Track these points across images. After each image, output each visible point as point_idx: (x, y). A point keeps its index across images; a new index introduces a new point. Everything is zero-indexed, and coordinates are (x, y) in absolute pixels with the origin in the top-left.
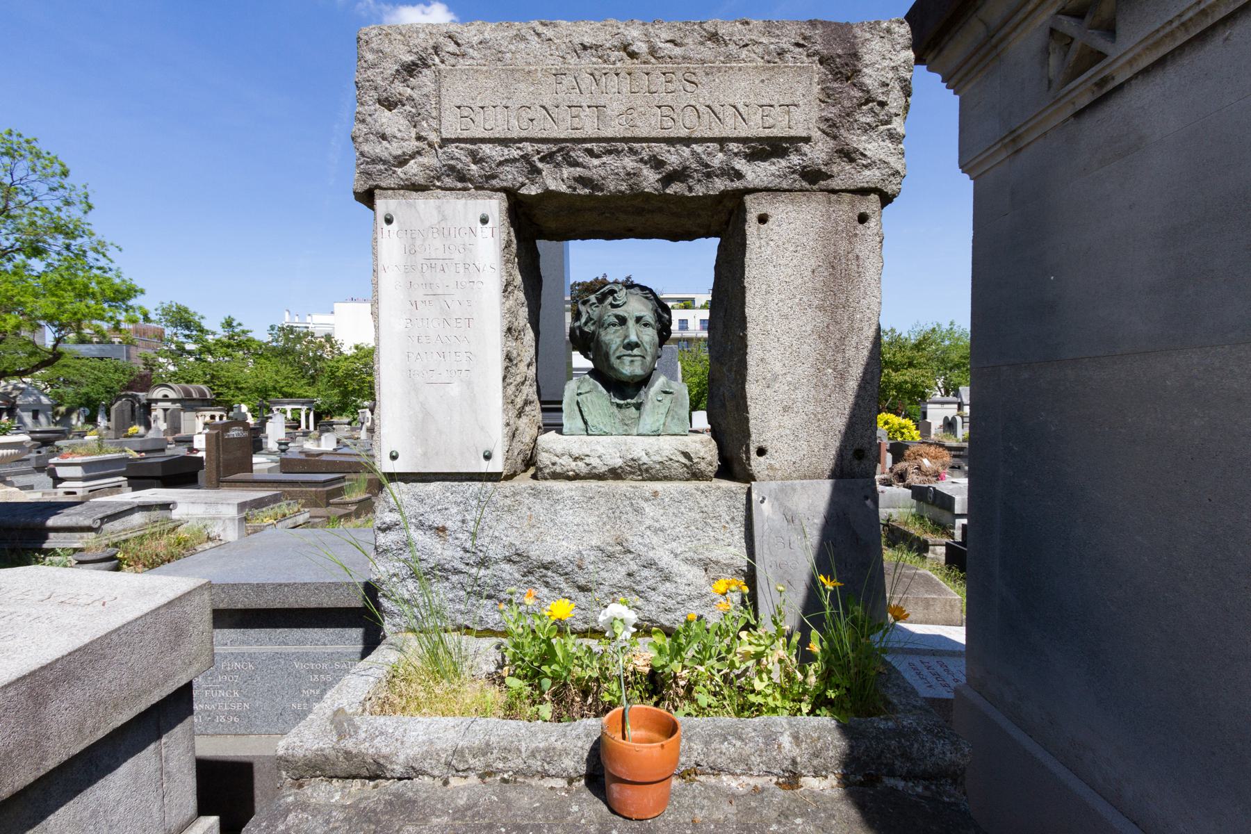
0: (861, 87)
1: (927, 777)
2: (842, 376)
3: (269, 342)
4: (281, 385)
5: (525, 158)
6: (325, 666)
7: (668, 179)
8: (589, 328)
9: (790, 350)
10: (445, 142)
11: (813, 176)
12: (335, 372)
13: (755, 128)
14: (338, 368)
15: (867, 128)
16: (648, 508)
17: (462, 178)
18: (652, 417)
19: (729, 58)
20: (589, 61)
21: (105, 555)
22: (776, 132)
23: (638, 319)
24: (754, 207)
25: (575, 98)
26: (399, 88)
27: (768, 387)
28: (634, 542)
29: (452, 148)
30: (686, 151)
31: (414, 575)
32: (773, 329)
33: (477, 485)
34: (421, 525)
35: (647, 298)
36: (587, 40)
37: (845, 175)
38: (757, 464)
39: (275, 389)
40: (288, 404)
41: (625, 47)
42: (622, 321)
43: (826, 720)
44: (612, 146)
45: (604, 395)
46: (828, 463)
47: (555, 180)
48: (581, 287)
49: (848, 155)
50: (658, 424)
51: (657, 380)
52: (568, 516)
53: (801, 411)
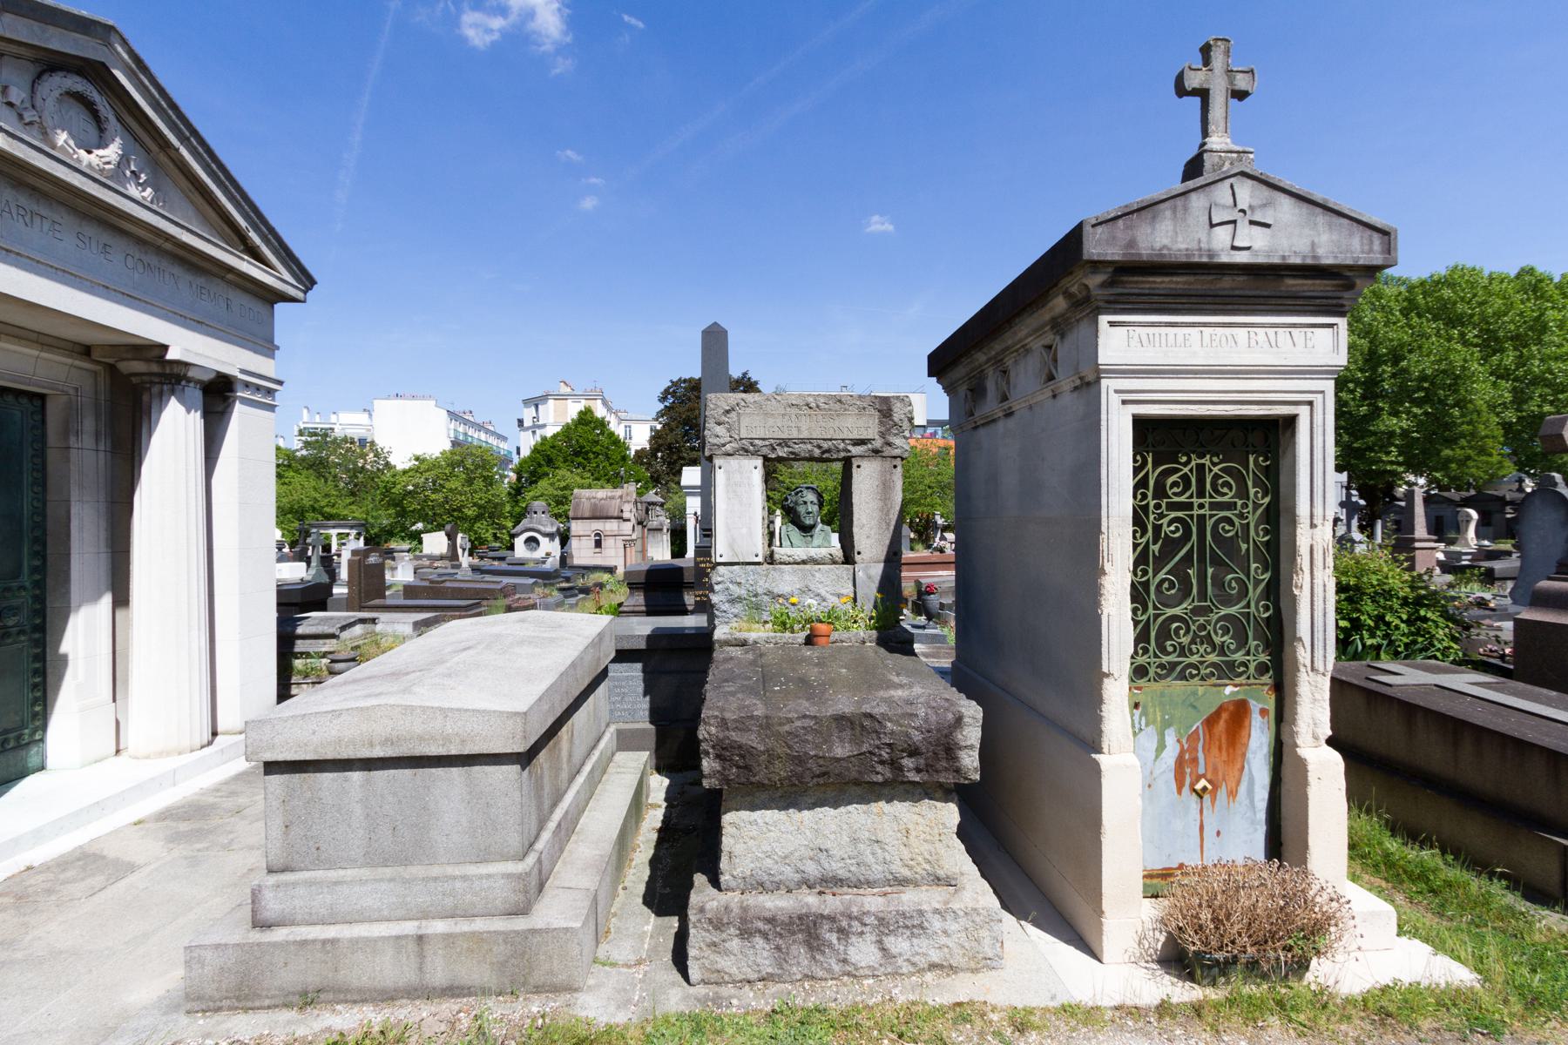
0: (893, 420)
1: (899, 643)
2: (888, 525)
3: (297, 450)
4: (323, 504)
5: (771, 445)
6: (624, 683)
7: (823, 453)
8: (791, 505)
10: (741, 439)
11: (876, 452)
12: (391, 488)
13: (855, 436)
15: (895, 435)
16: (817, 575)
17: (747, 451)
18: (817, 540)
19: (845, 410)
20: (794, 411)
21: (349, 657)
22: (862, 437)
24: (855, 462)
25: (790, 424)
26: (724, 418)
28: (812, 587)
29: (744, 441)
30: (830, 443)
31: (729, 601)
33: (752, 567)
34: (731, 582)
36: (794, 402)
37: (888, 451)
38: (857, 558)
39: (314, 509)
40: (334, 527)
41: (807, 405)
42: (805, 503)
43: (874, 632)
44: (803, 441)
46: (883, 558)
47: (782, 452)
48: (687, 384)
49: (889, 444)
52: (787, 577)
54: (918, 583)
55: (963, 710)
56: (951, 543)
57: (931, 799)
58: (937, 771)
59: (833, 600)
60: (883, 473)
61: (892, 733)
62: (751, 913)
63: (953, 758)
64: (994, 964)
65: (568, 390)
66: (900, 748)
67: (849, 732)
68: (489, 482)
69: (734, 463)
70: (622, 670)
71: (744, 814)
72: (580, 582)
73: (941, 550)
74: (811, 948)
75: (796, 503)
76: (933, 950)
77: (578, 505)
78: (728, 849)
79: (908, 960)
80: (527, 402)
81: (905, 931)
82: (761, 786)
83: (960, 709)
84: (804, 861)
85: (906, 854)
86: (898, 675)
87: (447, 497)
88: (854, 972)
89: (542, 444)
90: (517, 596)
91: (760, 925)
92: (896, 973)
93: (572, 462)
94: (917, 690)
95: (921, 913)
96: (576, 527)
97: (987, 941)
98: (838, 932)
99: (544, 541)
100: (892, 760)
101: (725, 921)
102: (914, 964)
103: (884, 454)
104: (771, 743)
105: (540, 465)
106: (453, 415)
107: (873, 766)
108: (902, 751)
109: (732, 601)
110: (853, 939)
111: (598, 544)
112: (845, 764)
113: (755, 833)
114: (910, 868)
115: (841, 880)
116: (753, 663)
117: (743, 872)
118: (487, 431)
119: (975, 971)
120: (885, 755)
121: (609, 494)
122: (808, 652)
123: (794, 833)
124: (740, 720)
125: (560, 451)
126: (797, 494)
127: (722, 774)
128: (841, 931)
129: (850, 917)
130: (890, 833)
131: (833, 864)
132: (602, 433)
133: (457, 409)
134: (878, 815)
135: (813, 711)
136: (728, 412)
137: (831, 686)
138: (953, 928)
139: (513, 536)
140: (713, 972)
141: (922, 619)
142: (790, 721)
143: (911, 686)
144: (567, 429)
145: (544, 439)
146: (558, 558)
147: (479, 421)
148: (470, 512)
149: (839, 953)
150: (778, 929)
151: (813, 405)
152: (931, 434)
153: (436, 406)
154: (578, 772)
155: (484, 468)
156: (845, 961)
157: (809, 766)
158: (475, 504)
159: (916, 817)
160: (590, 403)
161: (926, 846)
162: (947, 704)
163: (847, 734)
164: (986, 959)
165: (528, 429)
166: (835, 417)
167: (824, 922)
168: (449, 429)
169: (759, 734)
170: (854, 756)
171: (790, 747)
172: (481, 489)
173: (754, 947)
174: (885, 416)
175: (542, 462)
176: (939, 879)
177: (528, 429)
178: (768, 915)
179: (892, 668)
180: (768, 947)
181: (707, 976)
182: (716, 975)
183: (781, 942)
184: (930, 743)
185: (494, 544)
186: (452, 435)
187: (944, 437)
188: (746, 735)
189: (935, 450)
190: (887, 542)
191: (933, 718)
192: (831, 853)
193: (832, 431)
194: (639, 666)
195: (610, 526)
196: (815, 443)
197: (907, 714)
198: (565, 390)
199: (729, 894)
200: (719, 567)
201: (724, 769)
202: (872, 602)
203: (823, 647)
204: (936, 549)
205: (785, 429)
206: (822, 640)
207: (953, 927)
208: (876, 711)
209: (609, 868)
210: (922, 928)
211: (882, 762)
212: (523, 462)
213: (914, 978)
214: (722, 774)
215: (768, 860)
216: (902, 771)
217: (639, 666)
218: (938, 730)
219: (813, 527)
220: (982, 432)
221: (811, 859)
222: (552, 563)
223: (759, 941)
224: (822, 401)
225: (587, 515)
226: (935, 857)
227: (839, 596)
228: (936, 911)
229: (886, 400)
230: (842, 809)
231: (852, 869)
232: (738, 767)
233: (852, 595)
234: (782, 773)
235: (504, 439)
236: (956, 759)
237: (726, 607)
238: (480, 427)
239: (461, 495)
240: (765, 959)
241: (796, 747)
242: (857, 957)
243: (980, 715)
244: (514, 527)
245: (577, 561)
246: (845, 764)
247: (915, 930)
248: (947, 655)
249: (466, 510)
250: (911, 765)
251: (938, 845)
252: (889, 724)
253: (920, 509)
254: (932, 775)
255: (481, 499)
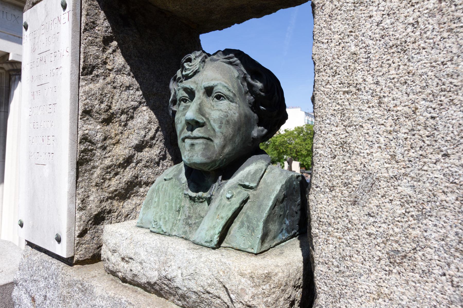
9: (409, 123)
14: (276, 141)
23: (209, 91)
27: (354, 203)
32: (370, 79)
35: (230, 63)
45: (181, 183)
50: (212, 232)
51: (248, 165)
53: (437, 271)
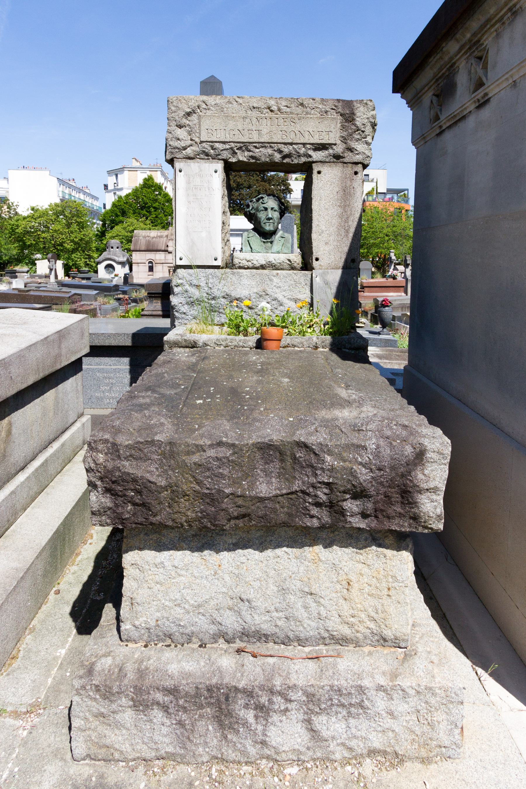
0: (355, 125)
2: (347, 231)
5: (232, 148)
6: (112, 375)
7: (284, 157)
10: (202, 142)
11: (337, 157)
12: (15, 229)
13: (316, 140)
15: (358, 140)
16: (275, 280)
17: (207, 155)
18: (276, 246)
19: (307, 113)
20: (255, 114)
26: (185, 121)
28: (269, 291)
29: (204, 144)
30: (291, 147)
31: (187, 303)
34: (191, 284)
37: (349, 157)
38: (315, 264)
41: (269, 108)
42: (266, 209)
44: (263, 145)
46: (341, 264)
47: (243, 156)
49: (351, 150)
54: (376, 300)
55: (426, 442)
56: (402, 273)
57: (380, 546)
58: (389, 517)
59: (290, 305)
60: (343, 179)
61: (332, 469)
62: (149, 681)
63: (410, 503)
64: (451, 753)
65: (137, 164)
66: (342, 489)
67: (277, 464)
68: (82, 226)
69: (194, 166)
70: (111, 363)
71: (149, 555)
72: (134, 295)
73: (394, 278)
74: (221, 725)
75: (257, 210)
76: (374, 733)
77: (137, 241)
78: (129, 594)
79: (343, 744)
80: (110, 173)
81: (340, 710)
82: (162, 526)
83: (422, 440)
84: (222, 611)
85: (346, 609)
86: (347, 387)
87: (52, 236)
88: (275, 756)
89: (118, 201)
90: (82, 303)
91: (159, 697)
92: (328, 759)
93: (139, 214)
94: (368, 410)
95: (361, 689)
96: (136, 257)
97: (443, 727)
98: (256, 709)
99: (118, 267)
100: (330, 502)
101: (115, 689)
102: (351, 749)
103: (345, 160)
104: (175, 476)
105: (117, 216)
106: (61, 182)
107: (306, 508)
108: (344, 492)
109: (191, 304)
110: (275, 718)
111: (151, 269)
112: (270, 505)
113: (161, 578)
114: (351, 626)
115: (266, 636)
116: (192, 367)
117: (146, 622)
118: (85, 193)
119: (425, 761)
120: (322, 495)
121: (159, 234)
122: (255, 357)
123: (210, 578)
124: (137, 447)
125: (130, 206)
126: (258, 200)
127: (114, 512)
128: (259, 707)
129: (272, 692)
130: (327, 585)
131: (256, 617)
132: (160, 194)
133: (64, 177)
134: (314, 561)
135: (231, 438)
136: (189, 114)
137: (264, 401)
138: (400, 709)
139: (99, 263)
140: (101, 747)
141: (378, 327)
142: (201, 449)
143: (360, 403)
144: (136, 191)
145: (120, 197)
146: (122, 278)
147: (79, 186)
148: (69, 246)
149: (256, 734)
150: (181, 702)
151: (274, 108)
152: (389, 198)
153: (50, 175)
154: (23, 469)
155: (78, 217)
156: (263, 743)
157: (224, 506)
158: (72, 241)
159: (361, 566)
160: (153, 174)
161: (372, 601)
162: (404, 433)
163: (275, 466)
164: (440, 747)
165: (111, 191)
166: (297, 121)
167: (240, 696)
168: (58, 191)
169: (161, 465)
170: (282, 495)
171: (199, 483)
172: (76, 231)
173: (151, 721)
174: (347, 121)
175: (119, 214)
176: (385, 640)
177: (111, 191)
178: (169, 683)
179: (342, 379)
180: (168, 722)
181: (94, 750)
182: (104, 750)
183: (184, 717)
184: (381, 483)
185: (84, 269)
186: (61, 195)
187: (398, 201)
188: (144, 465)
189: (392, 209)
190: (346, 249)
191: (386, 452)
192: (254, 604)
193: (292, 135)
194: (126, 360)
195: (159, 257)
196: (276, 147)
197: (353, 445)
198: (136, 164)
199: (130, 645)
200: (179, 271)
201: (117, 505)
202: (329, 308)
203: (272, 352)
204: (390, 276)
205: (246, 132)
206: (272, 345)
207: (400, 707)
208: (312, 440)
209: (27, 583)
210: (362, 707)
211: (318, 505)
212: (107, 213)
213: (349, 768)
214: (114, 512)
215: (178, 609)
216: (344, 515)
217: (126, 360)
218: (393, 468)
219: (274, 233)
220: (448, 136)
221: (230, 609)
222: (118, 281)
223: (157, 714)
224: (284, 103)
225: (143, 248)
226: (382, 615)
227: (296, 301)
228: (380, 688)
229: (349, 104)
230: (269, 553)
231: (279, 623)
232: (134, 504)
233: (309, 300)
234: (189, 513)
235: (97, 199)
236: (414, 504)
237: (185, 308)
238: (80, 190)
239: (62, 234)
240: (166, 736)
241: (207, 483)
242: (279, 739)
243: (448, 450)
244: (98, 257)
245: (136, 281)
246: (270, 505)
247: (353, 710)
248: (399, 358)
249: (66, 245)
250: (355, 509)
251: (386, 601)
252: (328, 458)
253: (380, 251)
254: (382, 522)
255: (76, 238)
